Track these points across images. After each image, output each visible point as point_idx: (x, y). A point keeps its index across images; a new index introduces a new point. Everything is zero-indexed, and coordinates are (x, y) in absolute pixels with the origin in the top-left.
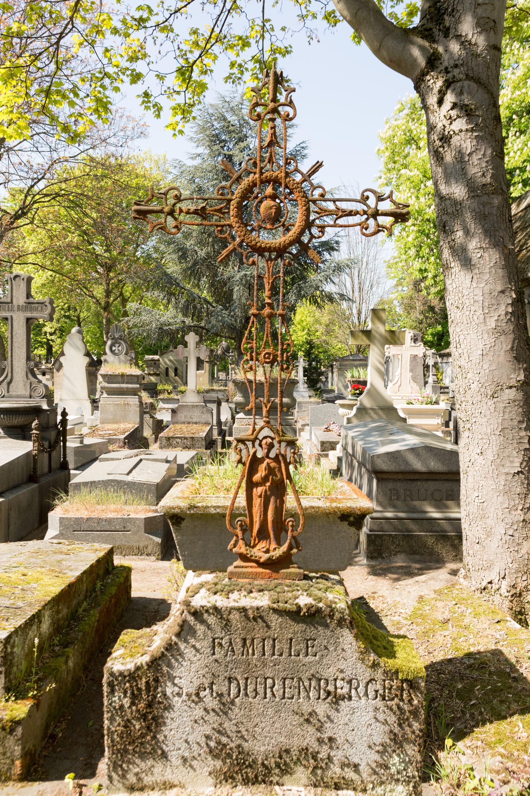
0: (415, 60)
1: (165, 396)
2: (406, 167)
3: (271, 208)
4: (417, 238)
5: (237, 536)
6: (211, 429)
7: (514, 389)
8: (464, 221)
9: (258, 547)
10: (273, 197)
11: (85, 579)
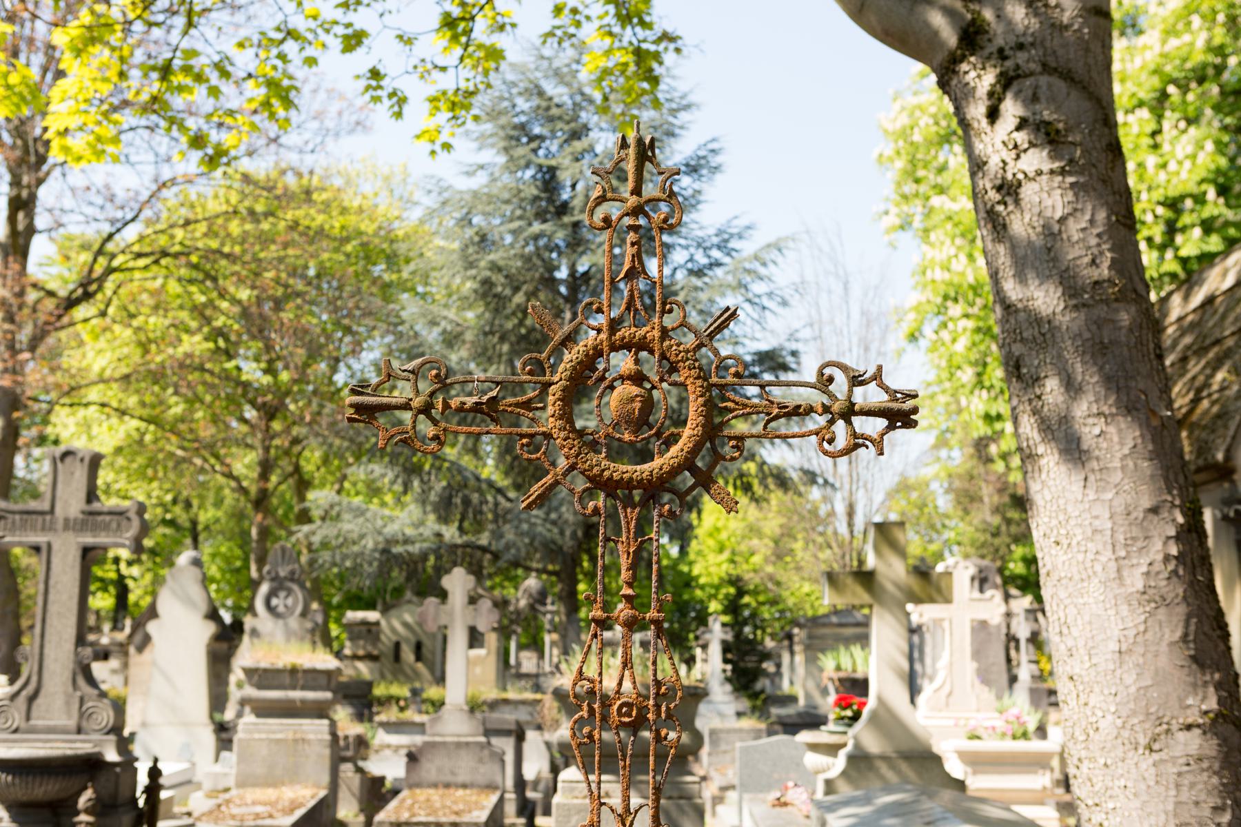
0: (936, 33)
1: (389, 714)
2: (942, 190)
3: (632, 400)
4: (974, 344)
7: (1197, 731)
8: (1060, 356)
10: (638, 378)
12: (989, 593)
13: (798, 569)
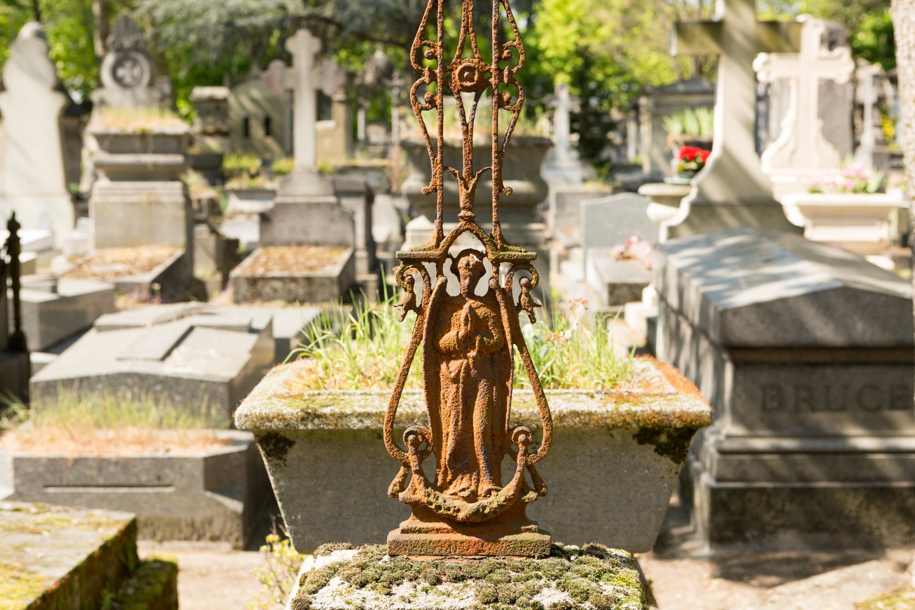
1: (243, 183)
5: (407, 466)
6: (352, 259)
9: (452, 489)
11: (76, 585)
12: (838, 51)
13: (647, 39)
